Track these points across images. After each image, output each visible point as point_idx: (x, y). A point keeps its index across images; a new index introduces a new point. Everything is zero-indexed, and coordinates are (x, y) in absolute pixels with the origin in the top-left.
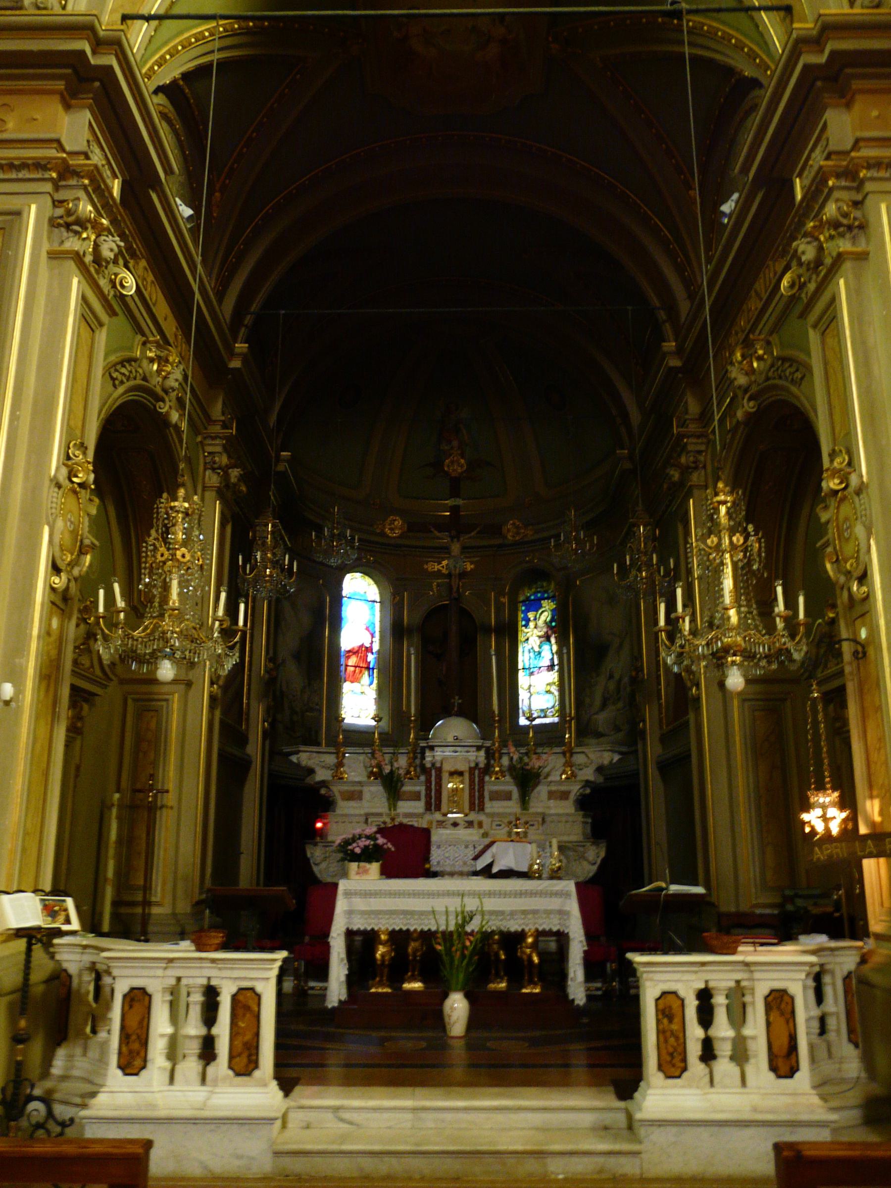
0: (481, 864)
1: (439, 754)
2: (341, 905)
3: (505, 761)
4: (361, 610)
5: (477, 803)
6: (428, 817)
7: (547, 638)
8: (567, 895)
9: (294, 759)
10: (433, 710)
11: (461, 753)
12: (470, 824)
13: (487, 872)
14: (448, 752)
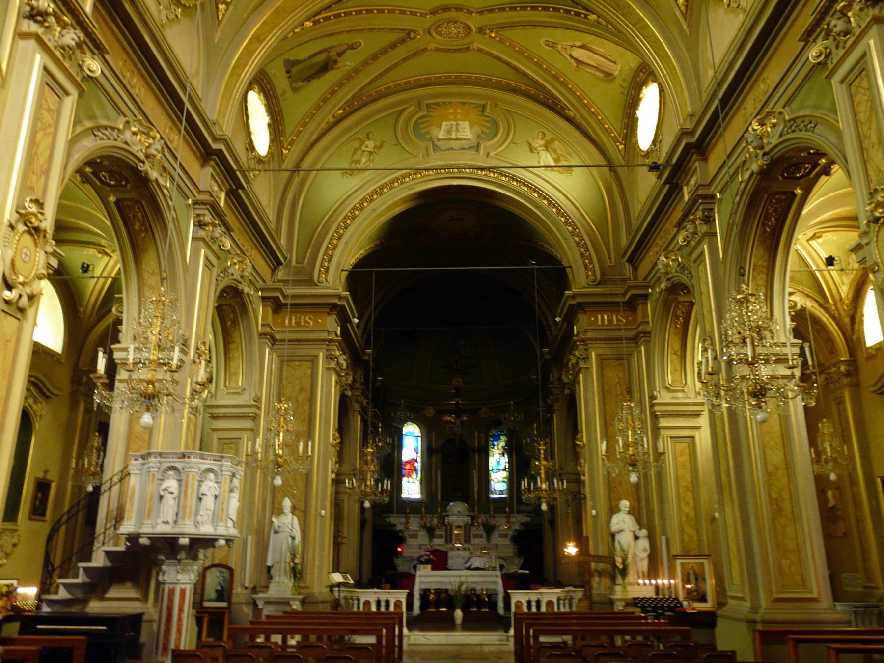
0: (467, 565)
1: (451, 518)
2: (418, 580)
3: (480, 521)
4: (412, 442)
5: (467, 540)
6: (447, 546)
7: (503, 455)
8: (497, 576)
9: (387, 520)
10: (447, 498)
11: (461, 518)
12: (464, 549)
13: (469, 568)
14: (455, 518)
